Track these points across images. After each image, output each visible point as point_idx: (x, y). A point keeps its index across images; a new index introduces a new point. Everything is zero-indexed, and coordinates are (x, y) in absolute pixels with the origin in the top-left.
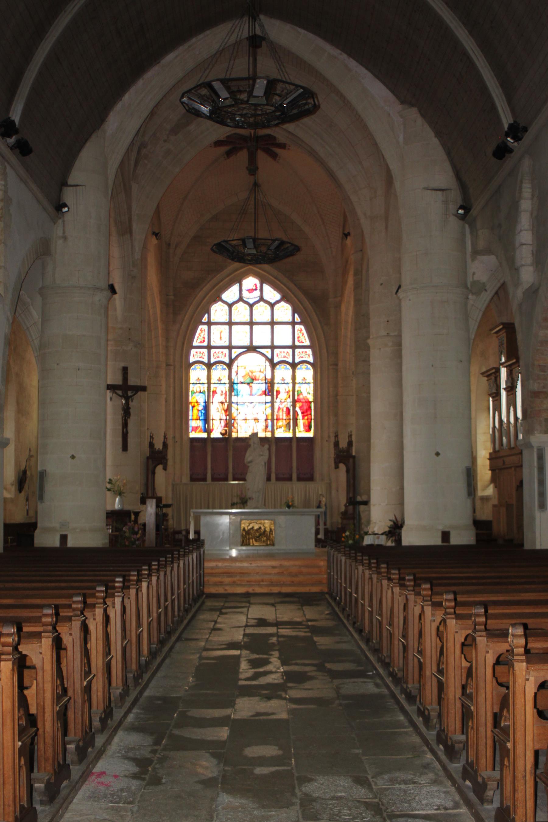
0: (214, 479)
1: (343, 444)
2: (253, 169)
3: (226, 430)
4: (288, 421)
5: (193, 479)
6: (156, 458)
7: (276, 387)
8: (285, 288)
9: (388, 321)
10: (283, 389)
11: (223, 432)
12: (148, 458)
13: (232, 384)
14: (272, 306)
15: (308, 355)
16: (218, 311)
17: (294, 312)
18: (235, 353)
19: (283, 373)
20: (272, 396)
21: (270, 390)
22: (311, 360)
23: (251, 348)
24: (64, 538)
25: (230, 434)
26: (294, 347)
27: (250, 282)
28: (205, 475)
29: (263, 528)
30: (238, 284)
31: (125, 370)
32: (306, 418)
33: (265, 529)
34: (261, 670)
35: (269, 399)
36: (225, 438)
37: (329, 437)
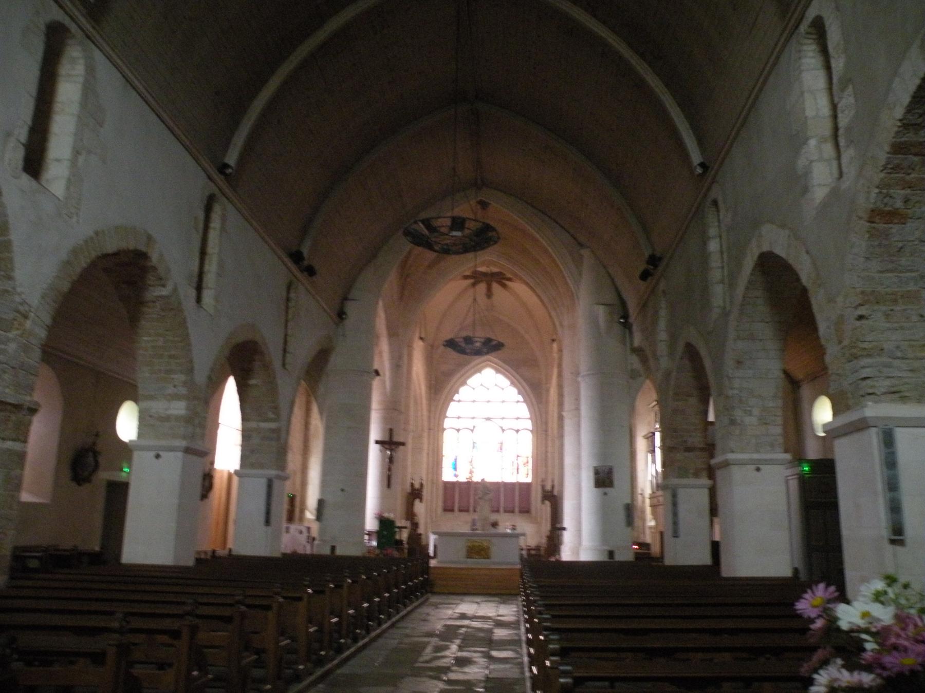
2: (489, 294)
6: (415, 494)
24: (333, 548)
31: (391, 430)
34: (439, 654)
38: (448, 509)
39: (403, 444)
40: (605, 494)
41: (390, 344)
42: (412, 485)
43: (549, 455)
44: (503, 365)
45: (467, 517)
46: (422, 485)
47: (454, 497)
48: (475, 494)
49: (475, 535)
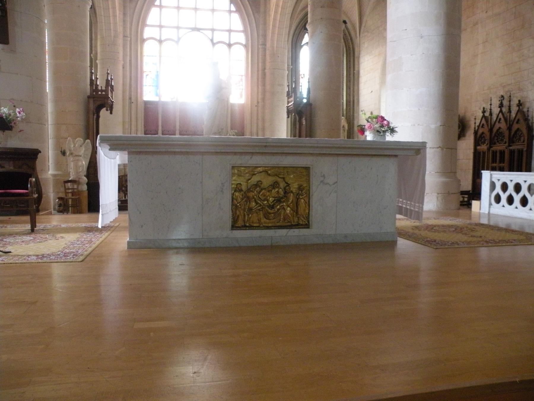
12: (89, 97)
15: (241, 38)
29: (282, 185)
46: (108, 83)
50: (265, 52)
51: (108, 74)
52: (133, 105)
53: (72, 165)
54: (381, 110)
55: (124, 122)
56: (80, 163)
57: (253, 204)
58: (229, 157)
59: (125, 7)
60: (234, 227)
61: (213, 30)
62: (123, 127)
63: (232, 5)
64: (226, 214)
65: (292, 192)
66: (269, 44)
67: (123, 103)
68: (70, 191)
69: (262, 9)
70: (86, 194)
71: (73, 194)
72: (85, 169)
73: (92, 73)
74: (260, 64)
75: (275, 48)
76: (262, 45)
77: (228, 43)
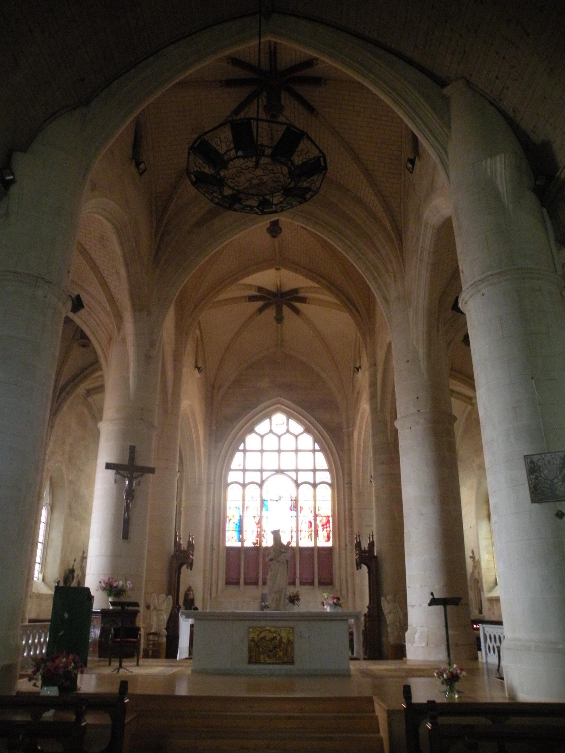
0: (246, 583)
1: (365, 545)
3: (257, 541)
4: (310, 533)
5: (228, 583)
7: (300, 504)
8: (307, 422)
9: (418, 398)
10: (306, 503)
11: (255, 542)
12: (172, 557)
13: (263, 501)
14: (296, 437)
15: (326, 477)
16: (252, 441)
17: (315, 440)
18: (265, 475)
19: (306, 491)
20: (297, 511)
21: (295, 506)
22: (329, 481)
23: (279, 471)
25: (261, 544)
26: (314, 470)
27: (279, 418)
28: (239, 579)
29: (278, 638)
30: (268, 420)
31: (132, 449)
32: (325, 530)
33: (281, 639)
35: (294, 513)
36: (257, 547)
37: (346, 545)
38: (232, 582)
39: (152, 471)
40: (560, 515)
41: (136, 322)
42: (177, 545)
43: (354, 512)
44: (294, 406)
45: (256, 592)
46: (191, 545)
47: (239, 566)
48: (264, 556)
49: (266, 617)
50: (351, 492)
51: (190, 536)
52: (215, 552)
53: (155, 618)
54: (480, 548)
55: (205, 571)
56: (162, 617)
57: (261, 649)
58: (247, 622)
59: (210, 455)
60: (249, 663)
61: (297, 471)
62: (204, 575)
63: (316, 444)
64: (245, 655)
65: (283, 642)
66: (354, 483)
67: (205, 551)
68: (151, 642)
69: (346, 448)
70: (164, 646)
71: (154, 645)
72: (166, 622)
73: (176, 535)
74: (347, 504)
75: (361, 488)
76: (348, 483)
77: (312, 482)
